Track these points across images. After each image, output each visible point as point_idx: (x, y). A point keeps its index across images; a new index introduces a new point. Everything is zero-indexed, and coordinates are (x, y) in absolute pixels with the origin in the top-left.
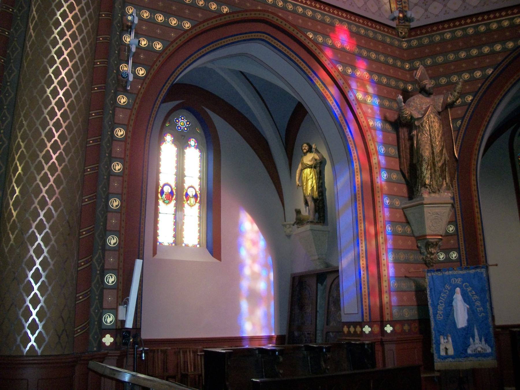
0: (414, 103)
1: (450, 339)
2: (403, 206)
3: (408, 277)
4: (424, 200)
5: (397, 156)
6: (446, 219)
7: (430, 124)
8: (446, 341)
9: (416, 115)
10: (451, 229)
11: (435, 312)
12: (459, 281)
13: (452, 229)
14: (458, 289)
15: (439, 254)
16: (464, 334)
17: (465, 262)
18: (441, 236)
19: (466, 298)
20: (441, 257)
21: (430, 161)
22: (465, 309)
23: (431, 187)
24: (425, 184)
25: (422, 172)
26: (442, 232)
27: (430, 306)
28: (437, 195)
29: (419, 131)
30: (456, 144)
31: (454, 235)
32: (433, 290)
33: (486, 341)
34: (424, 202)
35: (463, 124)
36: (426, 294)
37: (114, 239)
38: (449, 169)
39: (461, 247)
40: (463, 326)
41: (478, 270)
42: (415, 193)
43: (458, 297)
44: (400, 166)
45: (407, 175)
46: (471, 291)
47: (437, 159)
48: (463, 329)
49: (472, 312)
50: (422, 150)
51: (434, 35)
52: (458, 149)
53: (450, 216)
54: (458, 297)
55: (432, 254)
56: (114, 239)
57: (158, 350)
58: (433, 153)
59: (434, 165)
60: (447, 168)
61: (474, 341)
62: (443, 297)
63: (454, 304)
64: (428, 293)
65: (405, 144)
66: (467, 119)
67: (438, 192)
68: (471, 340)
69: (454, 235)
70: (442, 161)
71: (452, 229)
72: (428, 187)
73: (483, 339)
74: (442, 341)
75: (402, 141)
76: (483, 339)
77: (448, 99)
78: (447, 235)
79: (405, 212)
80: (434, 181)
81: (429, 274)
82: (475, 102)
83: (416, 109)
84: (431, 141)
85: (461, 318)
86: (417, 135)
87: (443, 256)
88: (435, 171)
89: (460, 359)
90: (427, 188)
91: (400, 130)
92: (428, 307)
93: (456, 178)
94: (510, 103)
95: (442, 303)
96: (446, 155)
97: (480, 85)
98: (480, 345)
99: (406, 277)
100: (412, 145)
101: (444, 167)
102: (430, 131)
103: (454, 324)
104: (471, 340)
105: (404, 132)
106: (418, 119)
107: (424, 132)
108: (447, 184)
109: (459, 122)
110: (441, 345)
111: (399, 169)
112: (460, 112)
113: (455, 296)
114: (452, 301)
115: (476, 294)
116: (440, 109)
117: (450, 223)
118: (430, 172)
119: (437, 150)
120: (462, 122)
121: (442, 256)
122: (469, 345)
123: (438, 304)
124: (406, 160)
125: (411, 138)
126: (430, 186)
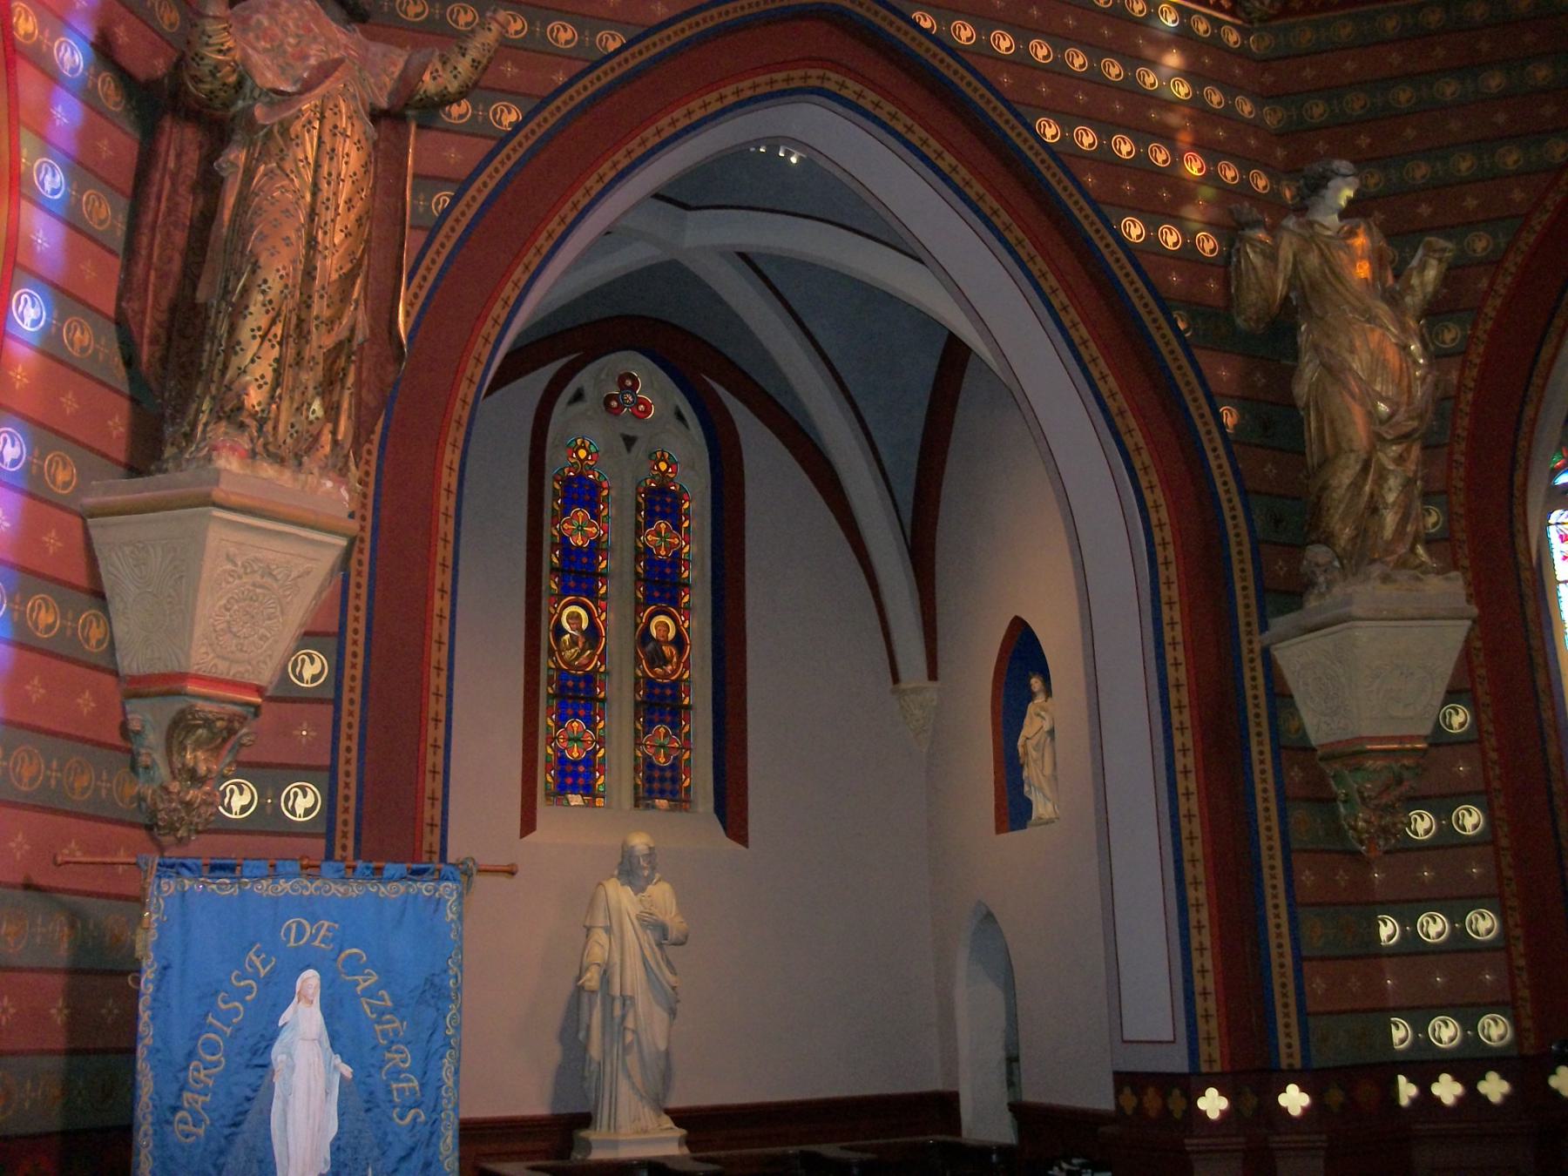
0: (272, 18)
2: (90, 501)
3: (38, 889)
4: (217, 482)
5: (119, 246)
6: (298, 610)
7: (327, 138)
9: (268, 76)
10: (309, 671)
13: (313, 669)
14: (310, 980)
15: (228, 785)
17: (351, 844)
18: (259, 690)
19: (342, 1030)
20: (238, 801)
21: (291, 303)
22: (329, 1083)
23: (269, 427)
24: (240, 408)
25: (233, 346)
26: (265, 676)
27: (142, 1065)
28: (286, 478)
29: (265, 154)
30: (408, 288)
31: (321, 701)
32: (174, 974)
34: (218, 494)
35: (456, 213)
36: (136, 994)
38: (359, 383)
39: (342, 768)
41: (424, 887)
42: (169, 451)
43: (304, 1020)
44: (120, 298)
45: (145, 353)
46: (370, 993)
47: (320, 308)
50: (263, 237)
52: (413, 317)
53: (324, 595)
54: (304, 1020)
55: (194, 777)
58: (309, 274)
59: (301, 331)
60: (352, 368)
63: (278, 1054)
64: (147, 986)
65: (174, 200)
66: (479, 192)
67: (292, 462)
69: (321, 701)
70: (341, 330)
71: (313, 669)
72: (254, 424)
75: (161, 182)
77: (427, 77)
78: (286, 695)
79: (94, 532)
80: (285, 405)
81: (169, 886)
82: (523, 143)
83: (277, 50)
84: (312, 214)
86: (249, 173)
87: (246, 800)
88: (299, 361)
90: (242, 426)
91: (167, 123)
92: (133, 1071)
93: (376, 437)
94: (576, 265)
96: (357, 318)
97: (561, 79)
99: (28, 886)
100: (208, 216)
101: (342, 362)
102: (318, 166)
105: (180, 145)
106: (279, 98)
107: (288, 166)
108: (335, 442)
109: (443, 198)
111: (110, 309)
112: (455, 157)
113: (286, 1016)
114: (269, 1047)
116: (383, 103)
117: (309, 637)
118: (276, 352)
119: (331, 266)
120: (455, 200)
121: (240, 800)
123: (191, 1055)
124: (163, 276)
125: (210, 184)
126: (262, 422)
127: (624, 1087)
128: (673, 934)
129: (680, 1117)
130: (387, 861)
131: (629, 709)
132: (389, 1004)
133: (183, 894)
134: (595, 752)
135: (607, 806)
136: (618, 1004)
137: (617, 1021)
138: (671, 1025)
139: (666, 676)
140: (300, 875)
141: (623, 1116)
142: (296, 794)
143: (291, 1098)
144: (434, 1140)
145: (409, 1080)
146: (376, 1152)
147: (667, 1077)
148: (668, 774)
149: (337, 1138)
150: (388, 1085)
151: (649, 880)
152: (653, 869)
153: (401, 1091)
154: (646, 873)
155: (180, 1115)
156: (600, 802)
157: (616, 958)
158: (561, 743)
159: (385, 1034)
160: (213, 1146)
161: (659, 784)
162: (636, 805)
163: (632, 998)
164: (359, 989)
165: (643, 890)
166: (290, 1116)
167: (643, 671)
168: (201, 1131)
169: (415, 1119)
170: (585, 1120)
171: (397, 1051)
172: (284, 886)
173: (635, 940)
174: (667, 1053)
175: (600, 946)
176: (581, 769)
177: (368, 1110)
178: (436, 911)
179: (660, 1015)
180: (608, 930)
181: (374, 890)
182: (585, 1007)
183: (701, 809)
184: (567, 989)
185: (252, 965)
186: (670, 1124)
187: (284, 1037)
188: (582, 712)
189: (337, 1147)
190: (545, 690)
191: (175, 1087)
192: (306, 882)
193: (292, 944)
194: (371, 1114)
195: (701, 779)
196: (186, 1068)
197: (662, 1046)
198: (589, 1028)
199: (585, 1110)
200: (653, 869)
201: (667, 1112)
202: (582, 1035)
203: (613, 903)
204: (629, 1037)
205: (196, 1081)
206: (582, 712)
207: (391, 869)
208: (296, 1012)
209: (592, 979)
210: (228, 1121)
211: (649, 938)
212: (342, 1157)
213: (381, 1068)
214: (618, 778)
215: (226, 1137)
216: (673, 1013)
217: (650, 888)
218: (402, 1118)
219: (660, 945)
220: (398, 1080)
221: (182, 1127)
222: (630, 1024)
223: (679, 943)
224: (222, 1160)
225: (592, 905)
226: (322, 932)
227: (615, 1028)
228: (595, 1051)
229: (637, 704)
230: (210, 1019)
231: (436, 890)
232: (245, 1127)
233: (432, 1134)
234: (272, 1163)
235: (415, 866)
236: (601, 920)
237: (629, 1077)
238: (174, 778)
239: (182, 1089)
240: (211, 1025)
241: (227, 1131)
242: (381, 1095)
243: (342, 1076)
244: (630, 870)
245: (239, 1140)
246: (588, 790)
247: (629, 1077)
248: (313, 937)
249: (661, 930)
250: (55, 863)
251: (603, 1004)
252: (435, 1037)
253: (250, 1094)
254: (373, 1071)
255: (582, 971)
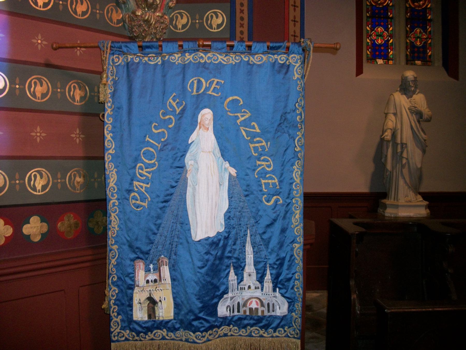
1: (166, 271)
8: (151, 277)
11: (127, 186)
12: (210, 85)
14: (206, 115)
16: (212, 258)
19: (229, 148)
33: (276, 284)
37: (217, 17)
40: (212, 234)
43: (204, 143)
46: (246, 123)
48: (213, 243)
49: (242, 192)
51: (423, 139)
54: (204, 143)
56: (217, 17)
57: (77, 102)
61: (240, 280)
62: (157, 137)
63: (189, 160)
68: (232, 276)
73: (268, 277)
74: (141, 276)
76: (268, 277)
85: (207, 206)
89: (192, 336)
95: (149, 156)
98: (258, 293)
103: (183, 223)
104: (232, 276)
110: (136, 290)
113: (193, 137)
114: (183, 156)
115: (263, 133)
122: (226, 292)
123: (137, 160)
127: (401, 182)
128: (425, 117)
129: (425, 196)
130: (254, 42)
131: (403, 22)
132: (258, 131)
133: (128, 64)
134: (388, 41)
135: (394, 64)
136: (399, 147)
137: (399, 154)
138: (423, 156)
139: (420, 6)
140: (198, 50)
141: (401, 195)
142: (212, 17)
143: (197, 187)
144: (288, 215)
145: (272, 178)
146: (252, 221)
147: (420, 178)
148: (421, 50)
149: (228, 211)
150: (260, 181)
151: (414, 92)
152: (416, 88)
153: (267, 185)
154: (413, 89)
155: (132, 194)
156: (391, 62)
157: (399, 126)
158: (373, 37)
159: (256, 149)
160: (153, 213)
161: (416, 55)
162: (407, 64)
163: (406, 144)
164: (238, 121)
165: (411, 97)
166: (197, 197)
167: (410, 5)
168: (145, 204)
169: (276, 201)
170: (385, 195)
171: (263, 160)
172: (189, 57)
173: (408, 120)
174: (421, 168)
175: (391, 122)
176: (382, 48)
177: (247, 196)
178: (286, 73)
179: (418, 152)
180: (395, 114)
181: (246, 59)
182: (385, 147)
183: (436, 65)
184: (378, 140)
185: (171, 106)
186: (421, 199)
187: (192, 149)
188: (382, 24)
189: (228, 217)
190: (366, 14)
191: (129, 178)
192: (202, 55)
193: (195, 93)
194: (248, 198)
195: (436, 52)
196: (135, 167)
197: (419, 166)
198: (386, 156)
199: (385, 191)
200: (416, 88)
201: (420, 193)
202: (383, 160)
203: (397, 103)
204: (404, 161)
205: (141, 175)
206: (382, 24)
207: (256, 46)
208: (198, 135)
209: (388, 135)
210: (161, 199)
211: (414, 118)
212: (232, 222)
213: (254, 170)
214: (398, 52)
215: (161, 209)
216: (424, 152)
217: (415, 96)
218: (268, 201)
219: (419, 122)
220: (265, 178)
221: (134, 201)
222: (405, 155)
223: (428, 120)
224: (159, 222)
225: (388, 103)
226: (214, 86)
227: (397, 157)
228: (389, 167)
229: (407, 19)
230: (147, 139)
231: (287, 59)
232: (171, 203)
233: (286, 212)
234: (188, 224)
235: (271, 45)
236: (392, 111)
237: (404, 178)
238: (138, 7)
239: (132, 180)
240: (148, 142)
241: (162, 205)
242: (254, 187)
243: (230, 175)
244: (405, 88)
245: (168, 210)
246: (386, 57)
247: (404, 178)
248: (207, 89)
249: (419, 114)
250: (52, 48)
251: (393, 145)
252: (288, 151)
253: (174, 184)
254: (248, 171)
255: (384, 132)
